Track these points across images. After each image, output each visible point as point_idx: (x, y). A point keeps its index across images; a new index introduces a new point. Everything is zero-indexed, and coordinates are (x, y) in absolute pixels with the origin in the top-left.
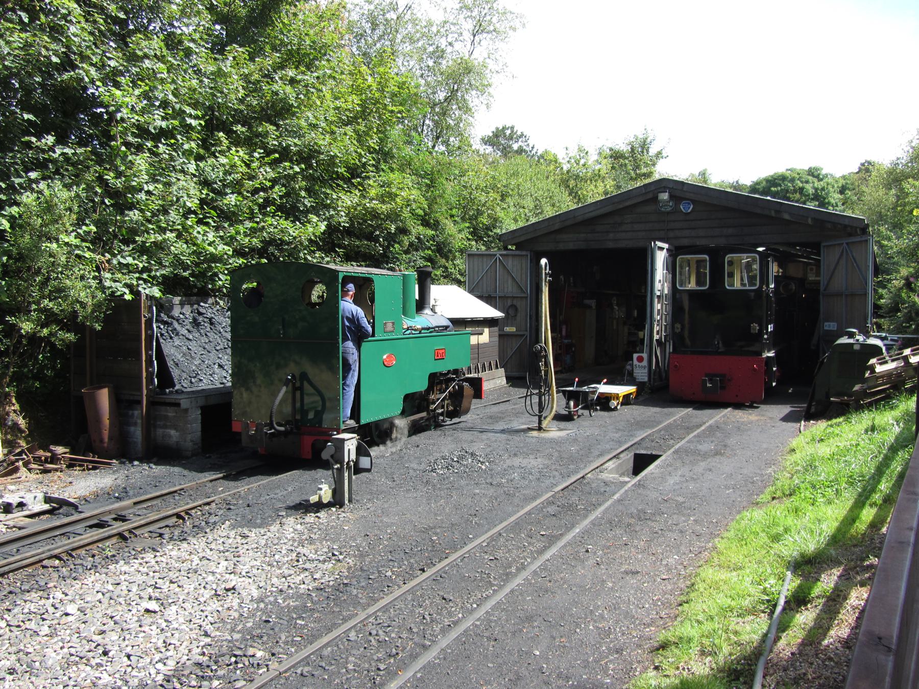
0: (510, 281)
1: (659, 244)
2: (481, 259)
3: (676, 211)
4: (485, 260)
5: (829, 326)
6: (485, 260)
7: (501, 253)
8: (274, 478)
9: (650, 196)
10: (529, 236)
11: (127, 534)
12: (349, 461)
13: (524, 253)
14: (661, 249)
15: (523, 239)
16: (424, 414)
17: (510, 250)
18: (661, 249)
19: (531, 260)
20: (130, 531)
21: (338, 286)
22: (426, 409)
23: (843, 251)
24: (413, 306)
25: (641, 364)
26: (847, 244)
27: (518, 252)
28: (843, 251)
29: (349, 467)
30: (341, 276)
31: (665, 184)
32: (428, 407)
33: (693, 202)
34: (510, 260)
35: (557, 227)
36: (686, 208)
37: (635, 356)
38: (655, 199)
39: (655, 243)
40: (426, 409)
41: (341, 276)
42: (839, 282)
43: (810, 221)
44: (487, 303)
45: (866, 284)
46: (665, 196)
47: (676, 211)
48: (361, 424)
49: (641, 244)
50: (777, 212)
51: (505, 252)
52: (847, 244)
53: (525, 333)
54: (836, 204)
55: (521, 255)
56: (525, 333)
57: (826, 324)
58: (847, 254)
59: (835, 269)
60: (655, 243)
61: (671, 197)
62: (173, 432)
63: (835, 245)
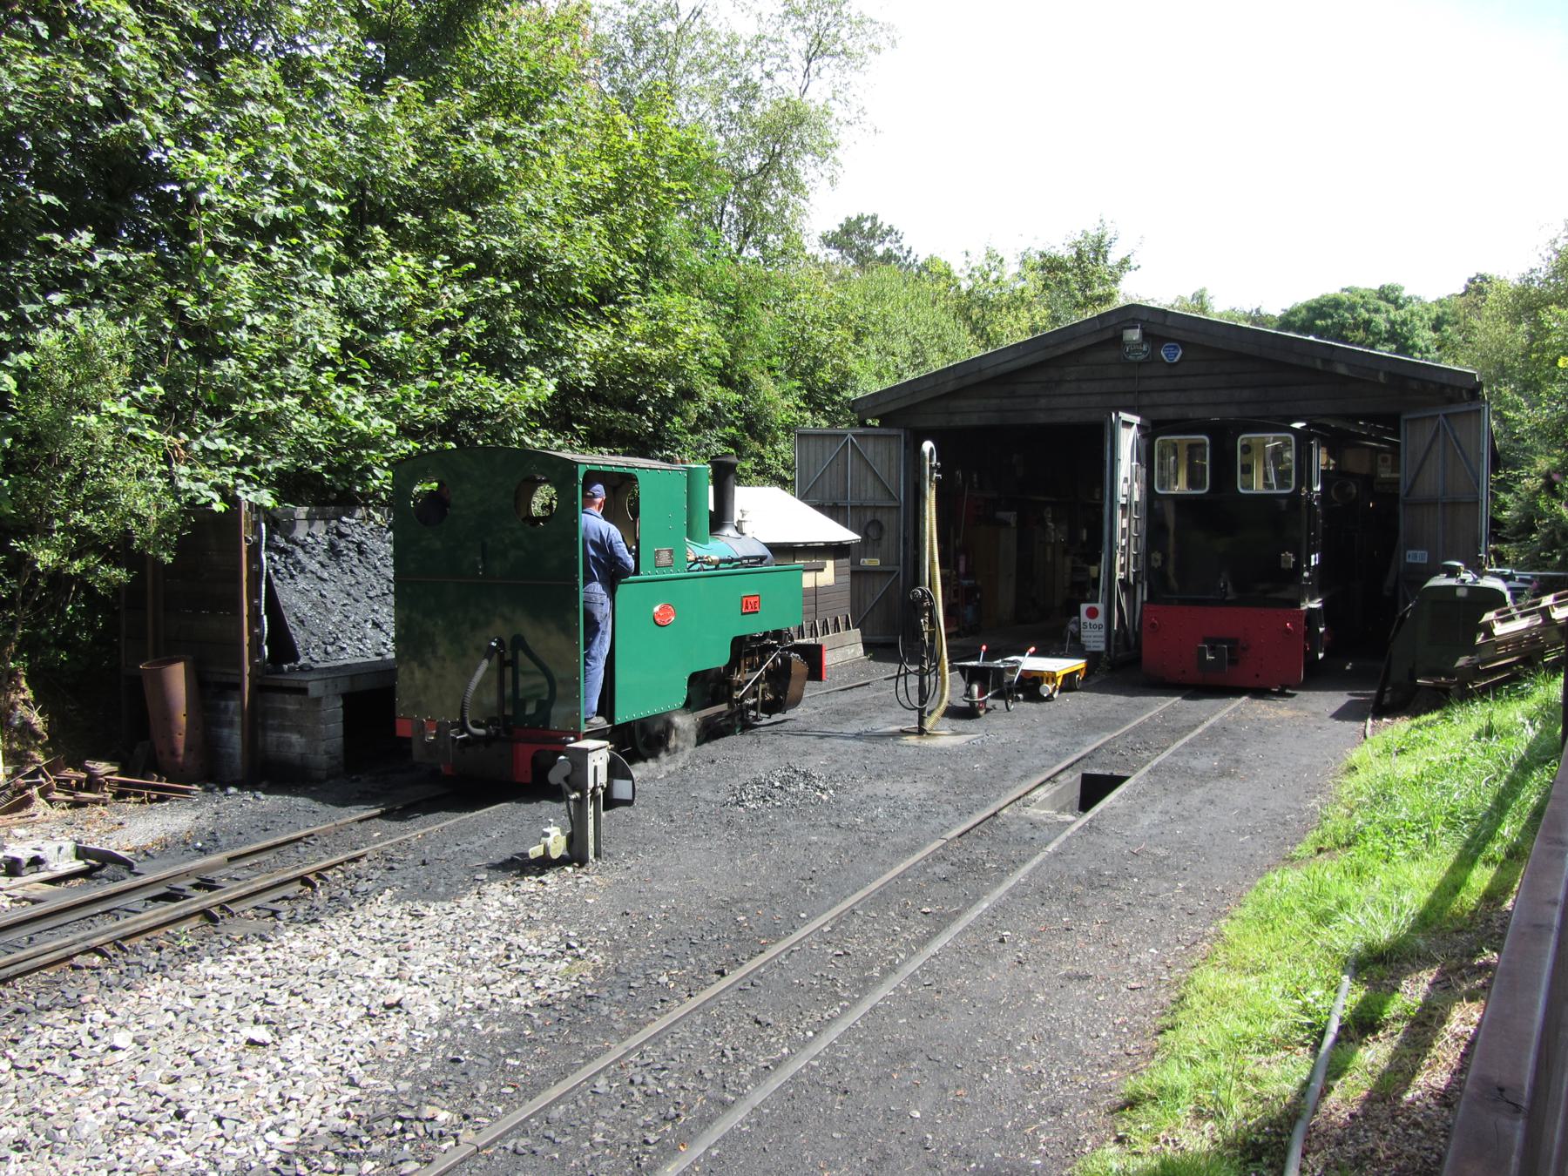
0: (870, 479)
1: (1125, 416)
2: (820, 443)
3: (1153, 360)
4: (828, 443)
5: (1415, 556)
6: (828, 443)
7: (855, 431)
8: (468, 816)
9: (1109, 334)
10: (903, 404)
11: (216, 912)
12: (595, 787)
13: (894, 432)
14: (1128, 424)
15: (892, 407)
16: (723, 707)
17: (870, 426)
18: (1128, 424)
19: (906, 444)
20: (222, 907)
21: (577, 488)
22: (727, 698)
23: (1438, 429)
24: (704, 523)
25: (1093, 622)
26: (1445, 416)
27: (883, 431)
28: (1438, 429)
29: (595, 798)
30: (581, 471)
31: (1134, 314)
32: (730, 694)
33: (1183, 344)
34: (870, 443)
35: (950, 387)
36: (1171, 355)
37: (1084, 607)
38: (1117, 340)
39: (1117, 414)
40: (727, 698)
41: (581, 471)
42: (1431, 482)
43: (1381, 377)
44: (831, 517)
45: (1478, 484)
46: (1134, 335)
47: (1153, 360)
48: (617, 723)
49: (1093, 416)
50: (1326, 361)
51: (861, 431)
52: (1445, 416)
53: (896, 568)
54: (1426, 349)
55: (890, 436)
56: (896, 568)
57: (1409, 552)
58: (1446, 434)
59: (1425, 458)
60: (1117, 414)
61: (1146, 336)
62: (295, 738)
63: (1425, 418)
